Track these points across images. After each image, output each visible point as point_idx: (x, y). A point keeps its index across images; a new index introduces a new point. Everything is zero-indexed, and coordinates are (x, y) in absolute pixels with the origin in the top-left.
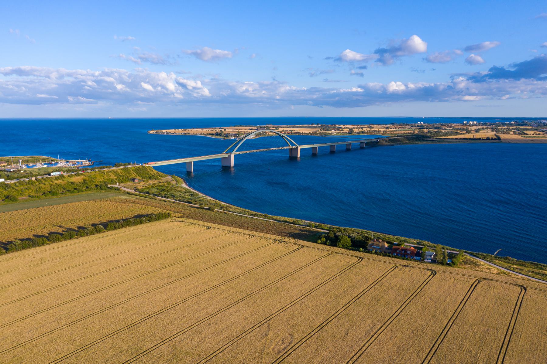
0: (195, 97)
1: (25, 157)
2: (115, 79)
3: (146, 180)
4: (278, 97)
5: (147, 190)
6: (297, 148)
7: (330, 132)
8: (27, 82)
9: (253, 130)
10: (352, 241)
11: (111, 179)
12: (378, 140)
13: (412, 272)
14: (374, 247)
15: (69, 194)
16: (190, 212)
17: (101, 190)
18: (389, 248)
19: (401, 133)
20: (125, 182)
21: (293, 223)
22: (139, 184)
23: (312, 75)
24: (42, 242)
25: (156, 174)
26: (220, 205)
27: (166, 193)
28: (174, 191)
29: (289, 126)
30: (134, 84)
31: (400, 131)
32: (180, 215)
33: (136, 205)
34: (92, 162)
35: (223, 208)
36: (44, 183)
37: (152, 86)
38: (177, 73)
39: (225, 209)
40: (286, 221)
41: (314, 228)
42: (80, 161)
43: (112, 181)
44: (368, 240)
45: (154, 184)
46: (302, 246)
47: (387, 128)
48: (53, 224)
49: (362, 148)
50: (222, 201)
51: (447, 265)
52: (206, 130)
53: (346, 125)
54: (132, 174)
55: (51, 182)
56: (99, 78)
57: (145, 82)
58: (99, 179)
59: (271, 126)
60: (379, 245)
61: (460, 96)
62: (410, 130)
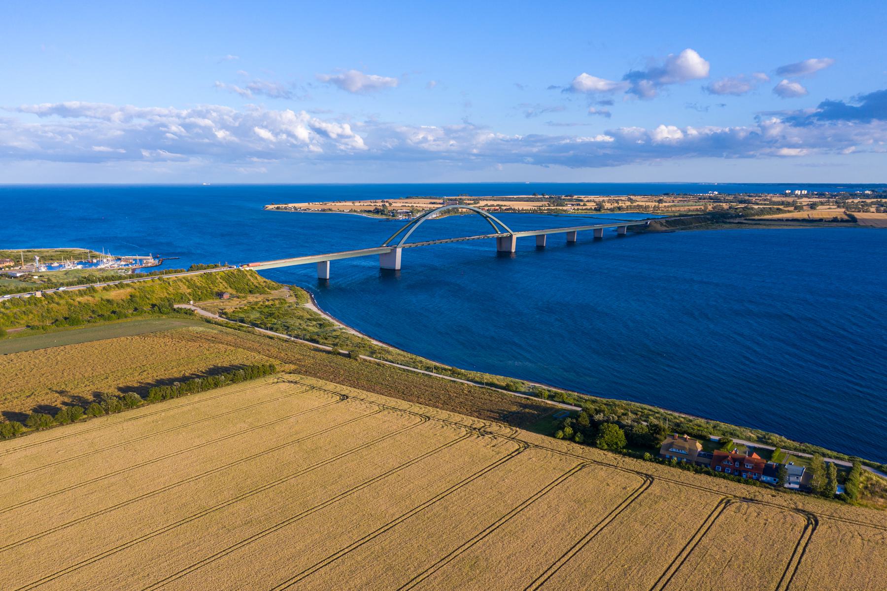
0: (342, 150)
1: (48, 251)
2: (214, 121)
3: (243, 295)
4: (475, 151)
5: (242, 315)
6: (511, 236)
7: (565, 208)
8: (76, 127)
9: (437, 204)
10: (627, 435)
11: (181, 294)
13: (765, 517)
14: (674, 450)
15: (102, 322)
16: (312, 361)
17: (160, 315)
18: (704, 454)
19: (683, 209)
20: (205, 300)
21: (507, 388)
22: (230, 304)
23: (528, 115)
24: (12, 430)
25: (261, 283)
26: (370, 347)
27: (276, 321)
28: (290, 317)
29: (495, 197)
30: (243, 130)
31: (682, 206)
32: (292, 367)
33: (216, 346)
34: (159, 260)
35: (375, 353)
36: (57, 301)
37: (272, 134)
38: (313, 112)
39: (379, 355)
40: (492, 385)
41: (548, 399)
42: (138, 257)
43: (182, 298)
44: (658, 433)
45: (257, 303)
46: (527, 446)
47: (660, 201)
48: (50, 386)
49: (621, 236)
50: (374, 339)
51: (837, 500)
52: (360, 204)
53: (589, 196)
54: (219, 285)
55: (71, 299)
56: (187, 121)
57: (263, 127)
58: (159, 294)
59: (467, 197)
60: (684, 448)
61: (773, 149)
62: (699, 205)
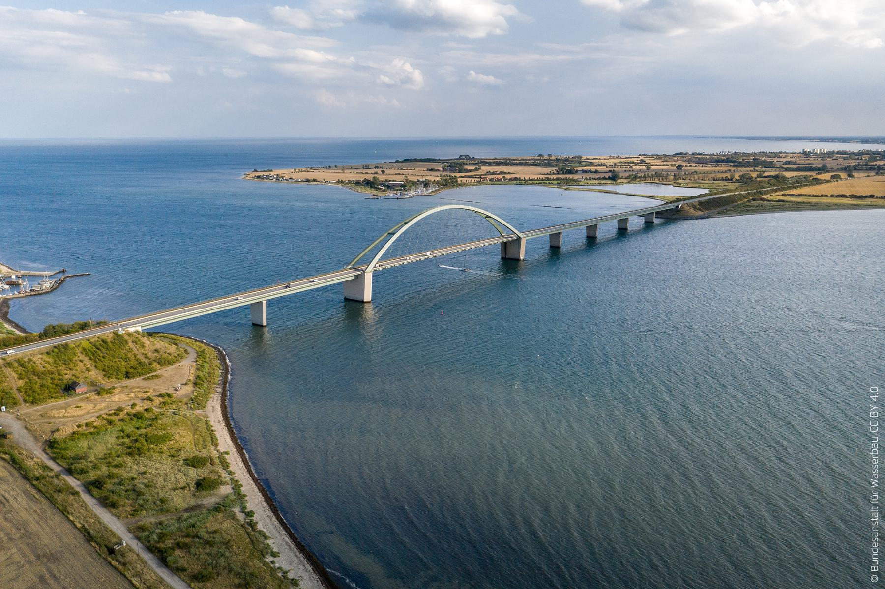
6: (519, 239)
12: (680, 206)
